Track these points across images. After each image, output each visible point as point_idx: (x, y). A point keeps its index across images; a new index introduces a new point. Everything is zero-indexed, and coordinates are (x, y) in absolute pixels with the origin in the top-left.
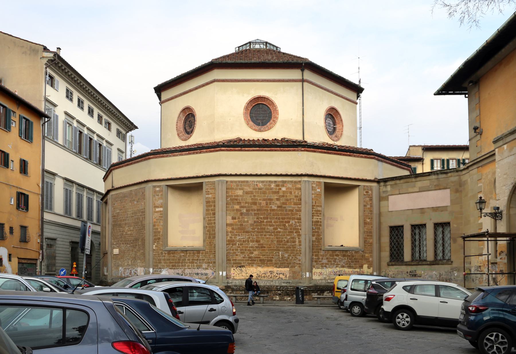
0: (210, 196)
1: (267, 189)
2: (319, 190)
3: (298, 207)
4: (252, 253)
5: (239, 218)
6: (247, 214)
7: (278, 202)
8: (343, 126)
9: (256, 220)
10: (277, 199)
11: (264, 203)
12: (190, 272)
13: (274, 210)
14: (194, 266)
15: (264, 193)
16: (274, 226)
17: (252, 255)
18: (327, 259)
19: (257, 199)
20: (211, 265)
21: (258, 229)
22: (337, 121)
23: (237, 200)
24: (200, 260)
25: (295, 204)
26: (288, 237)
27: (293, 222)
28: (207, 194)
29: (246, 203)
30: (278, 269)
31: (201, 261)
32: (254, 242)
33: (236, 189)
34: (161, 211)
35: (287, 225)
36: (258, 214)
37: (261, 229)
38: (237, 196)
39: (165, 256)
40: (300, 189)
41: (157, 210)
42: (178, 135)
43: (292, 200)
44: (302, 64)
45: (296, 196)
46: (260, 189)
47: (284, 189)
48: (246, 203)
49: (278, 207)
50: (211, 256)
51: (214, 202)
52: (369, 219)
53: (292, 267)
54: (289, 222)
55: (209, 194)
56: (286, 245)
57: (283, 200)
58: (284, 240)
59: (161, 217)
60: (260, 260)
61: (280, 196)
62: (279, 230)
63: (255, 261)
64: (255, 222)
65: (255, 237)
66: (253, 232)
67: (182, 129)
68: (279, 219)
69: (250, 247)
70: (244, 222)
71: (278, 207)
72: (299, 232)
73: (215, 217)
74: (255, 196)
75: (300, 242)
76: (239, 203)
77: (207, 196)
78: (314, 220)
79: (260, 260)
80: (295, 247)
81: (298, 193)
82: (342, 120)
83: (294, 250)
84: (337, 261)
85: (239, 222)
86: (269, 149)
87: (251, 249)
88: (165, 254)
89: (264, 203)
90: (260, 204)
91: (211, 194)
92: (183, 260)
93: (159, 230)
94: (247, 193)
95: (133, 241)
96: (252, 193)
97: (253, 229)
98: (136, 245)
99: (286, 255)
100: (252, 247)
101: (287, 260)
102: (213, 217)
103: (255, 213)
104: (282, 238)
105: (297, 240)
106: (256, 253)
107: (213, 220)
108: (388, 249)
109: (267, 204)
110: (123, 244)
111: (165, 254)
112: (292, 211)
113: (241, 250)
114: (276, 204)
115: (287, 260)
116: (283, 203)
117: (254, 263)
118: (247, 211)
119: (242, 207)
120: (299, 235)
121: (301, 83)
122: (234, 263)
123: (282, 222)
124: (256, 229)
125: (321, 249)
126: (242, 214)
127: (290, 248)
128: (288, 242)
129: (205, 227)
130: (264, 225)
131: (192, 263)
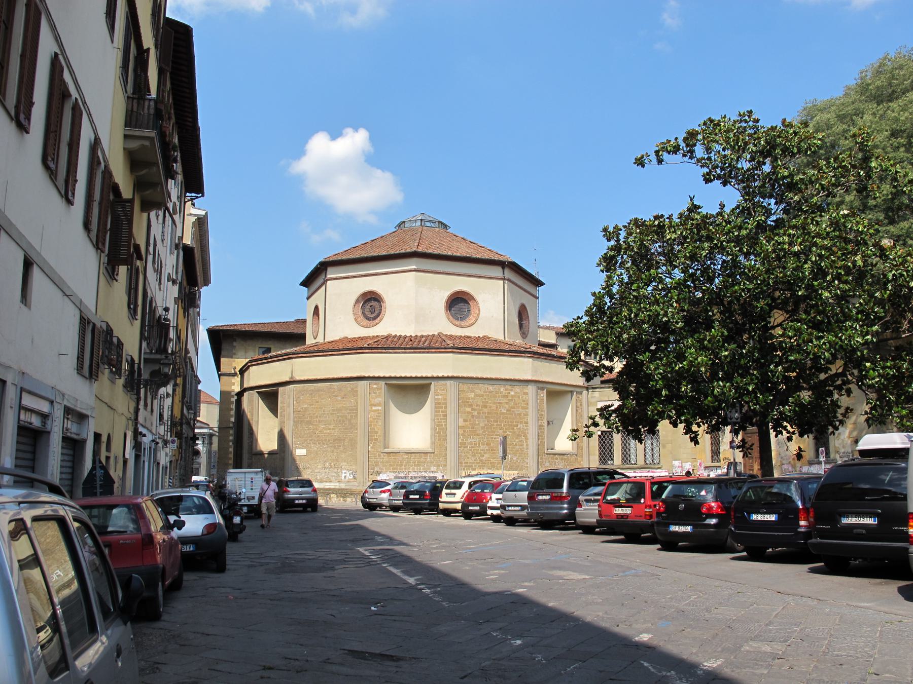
1: (496, 392)
11: (494, 406)
15: (495, 396)
40: (527, 394)
41: (374, 408)
42: (356, 320)
47: (512, 393)
51: (446, 403)
57: (512, 404)
76: (471, 406)
89: (494, 406)
94: (478, 396)
96: (482, 396)
106: (486, 455)
116: (513, 408)
120: (527, 439)
126: (473, 416)
129: (432, 429)
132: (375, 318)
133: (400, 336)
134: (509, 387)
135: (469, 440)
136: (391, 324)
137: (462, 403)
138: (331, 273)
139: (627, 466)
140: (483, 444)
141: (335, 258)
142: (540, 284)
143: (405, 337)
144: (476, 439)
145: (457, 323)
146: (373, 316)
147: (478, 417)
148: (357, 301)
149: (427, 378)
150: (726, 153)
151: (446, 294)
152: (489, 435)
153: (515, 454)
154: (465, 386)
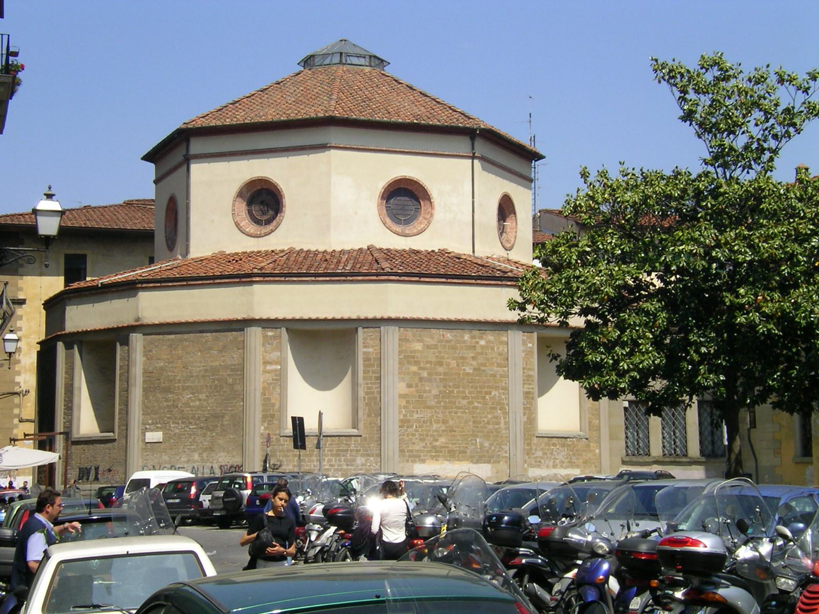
47: (482, 343)
57: (481, 359)
76: (417, 363)
89: (453, 363)
94: (428, 347)
96: (436, 347)
120: (506, 414)
126: (421, 379)
132: (268, 222)
133: (309, 251)
134: (476, 333)
135: (415, 416)
136: (290, 235)
137: (407, 358)
138: (197, 146)
139: (640, 459)
140: (437, 422)
141: (205, 123)
142: (538, 157)
143: (316, 253)
144: (428, 414)
145: (399, 229)
146: (265, 217)
147: (429, 380)
148: (240, 194)
149: (350, 320)
150: (342, 460)
151: (381, 184)
152: (445, 408)
153: (487, 437)
154: (410, 333)
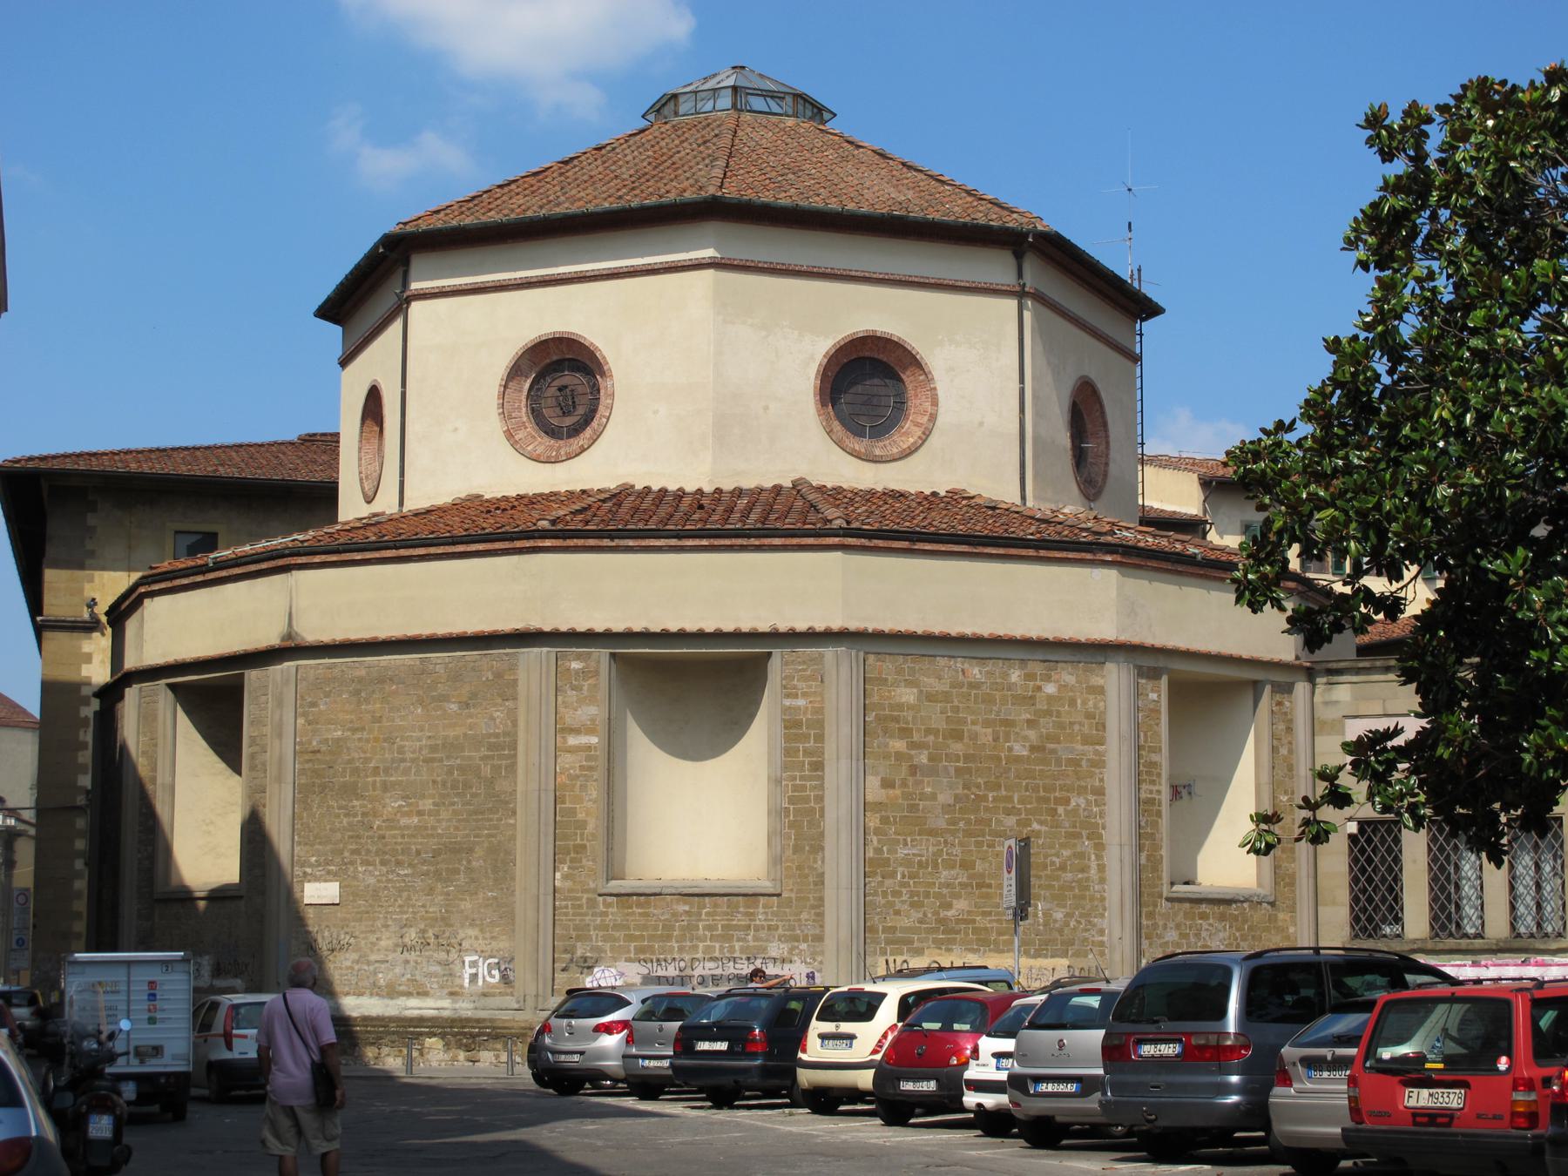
0: (801, 702)
2: (1153, 696)
3: (1097, 752)
4: (949, 906)
5: (904, 784)
6: (932, 771)
7: (1032, 734)
8: (1108, 443)
9: (960, 791)
10: (1028, 721)
11: (985, 736)
12: (718, 972)
13: (1018, 759)
14: (732, 950)
16: (1019, 812)
17: (950, 914)
18: (1178, 926)
19: (964, 721)
20: (804, 946)
21: (968, 822)
22: (1089, 426)
23: (896, 719)
24: (757, 929)
25: (1086, 741)
26: (1066, 853)
27: (1082, 801)
28: (788, 696)
29: (928, 731)
30: (1032, 962)
31: (763, 934)
32: (953, 867)
33: (896, 684)
34: (589, 748)
35: (1061, 810)
36: (969, 771)
37: (979, 822)
38: (900, 707)
39: (605, 914)
41: (572, 741)
42: (509, 435)
43: (1077, 727)
44: (1026, 235)
45: (1090, 716)
46: (975, 685)
48: (928, 731)
49: (1033, 749)
50: (804, 916)
51: (820, 724)
52: (1286, 793)
53: (1077, 954)
54: (1067, 801)
55: (796, 696)
56: (1058, 878)
58: (1053, 863)
59: (591, 768)
60: (976, 931)
61: (1036, 712)
62: (1036, 826)
63: (958, 932)
64: (957, 798)
65: (957, 850)
66: (953, 833)
67: (523, 414)
68: (1036, 789)
69: (941, 886)
70: (923, 797)
71: (1033, 749)
72: (1100, 836)
73: (822, 778)
74: (956, 710)
75: (1102, 868)
76: (905, 732)
77: (787, 702)
78: (1143, 795)
79: (976, 931)
80: (1087, 888)
81: (1095, 706)
82: (1105, 424)
83: (1083, 897)
84: (1204, 934)
85: (906, 796)
86: (1001, 551)
87: (945, 891)
88: (607, 905)
89: (985, 736)
90: (974, 737)
91: (805, 695)
92: (682, 928)
93: (581, 816)
94: (931, 698)
95: (436, 854)
96: (946, 697)
97: (953, 822)
98: (457, 871)
99: (1059, 915)
100: (948, 885)
101: (1061, 931)
102: (810, 778)
103: (957, 770)
104: (1046, 857)
105: (1094, 865)
107: (814, 788)
108: (1344, 895)
109: (996, 739)
110: (366, 863)
111: (607, 905)
112: (1075, 763)
113: (912, 894)
114: (1026, 738)
115: (1061, 931)
117: (953, 941)
118: (931, 759)
119: (913, 745)
121: (1012, 304)
122: (888, 942)
123: (1047, 800)
124: (961, 824)
125: (1161, 896)
126: (914, 770)
127: (1072, 889)
128: (1063, 868)
129: (776, 813)
130: (987, 809)
131: (725, 938)
